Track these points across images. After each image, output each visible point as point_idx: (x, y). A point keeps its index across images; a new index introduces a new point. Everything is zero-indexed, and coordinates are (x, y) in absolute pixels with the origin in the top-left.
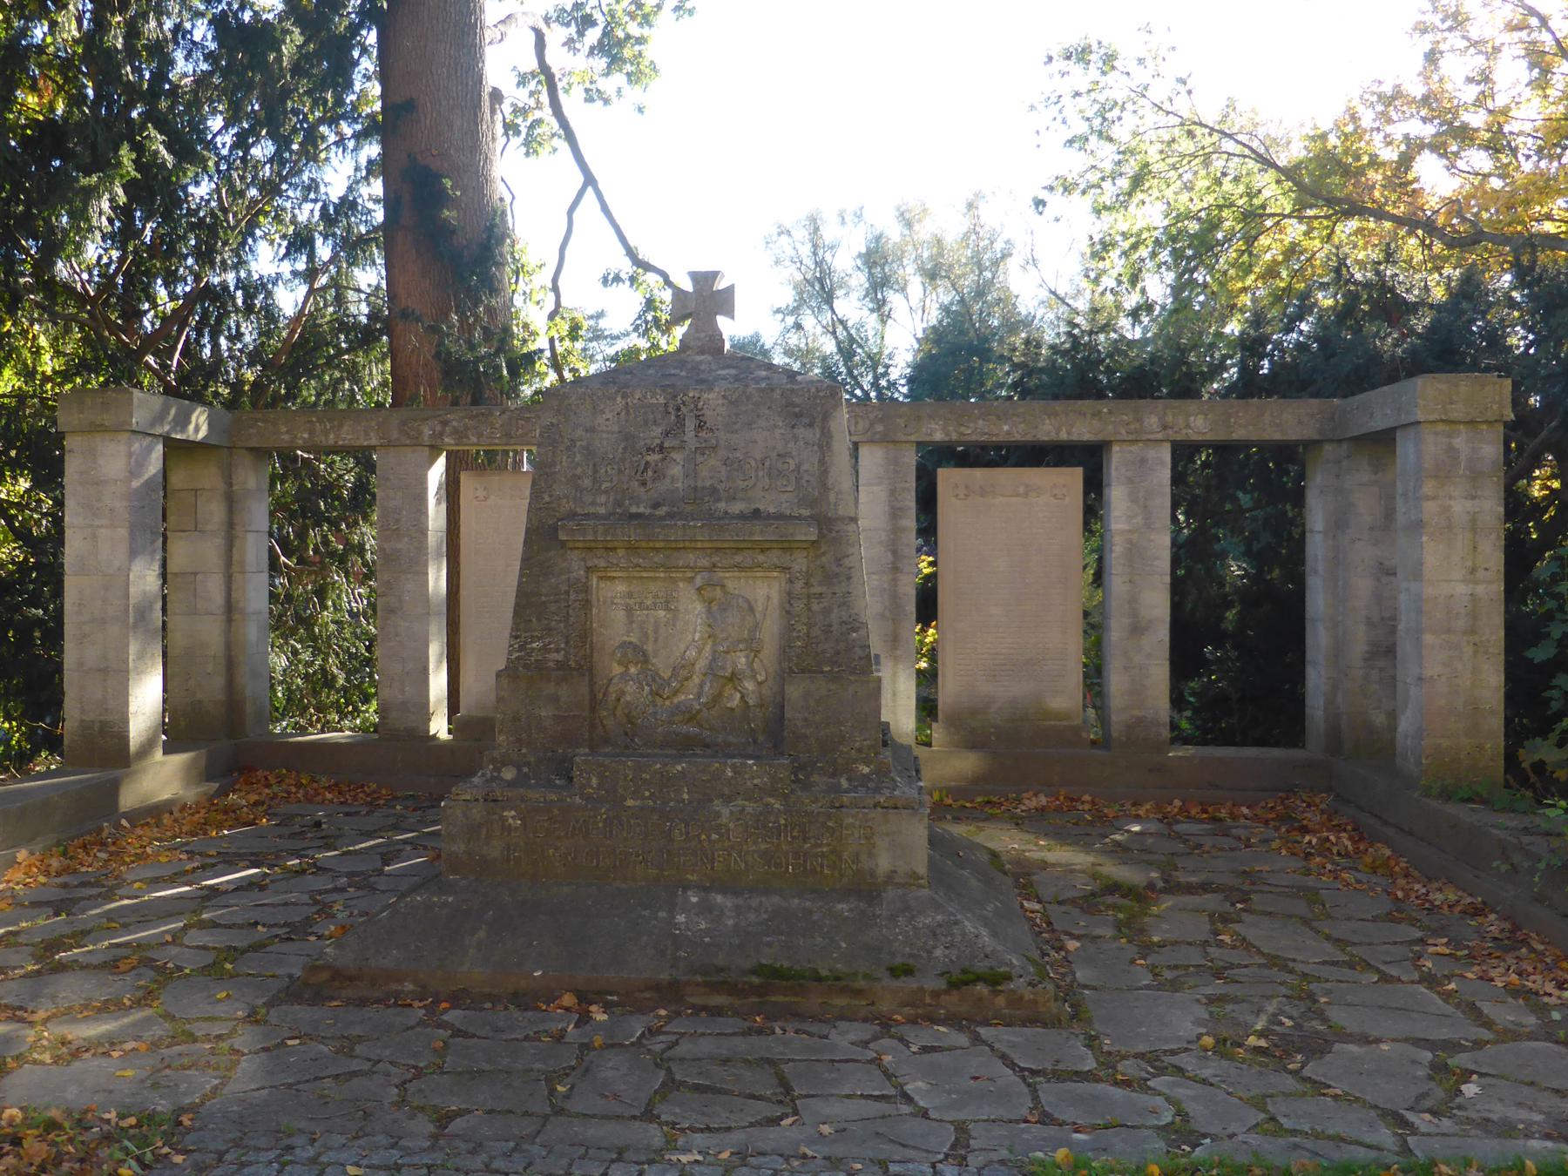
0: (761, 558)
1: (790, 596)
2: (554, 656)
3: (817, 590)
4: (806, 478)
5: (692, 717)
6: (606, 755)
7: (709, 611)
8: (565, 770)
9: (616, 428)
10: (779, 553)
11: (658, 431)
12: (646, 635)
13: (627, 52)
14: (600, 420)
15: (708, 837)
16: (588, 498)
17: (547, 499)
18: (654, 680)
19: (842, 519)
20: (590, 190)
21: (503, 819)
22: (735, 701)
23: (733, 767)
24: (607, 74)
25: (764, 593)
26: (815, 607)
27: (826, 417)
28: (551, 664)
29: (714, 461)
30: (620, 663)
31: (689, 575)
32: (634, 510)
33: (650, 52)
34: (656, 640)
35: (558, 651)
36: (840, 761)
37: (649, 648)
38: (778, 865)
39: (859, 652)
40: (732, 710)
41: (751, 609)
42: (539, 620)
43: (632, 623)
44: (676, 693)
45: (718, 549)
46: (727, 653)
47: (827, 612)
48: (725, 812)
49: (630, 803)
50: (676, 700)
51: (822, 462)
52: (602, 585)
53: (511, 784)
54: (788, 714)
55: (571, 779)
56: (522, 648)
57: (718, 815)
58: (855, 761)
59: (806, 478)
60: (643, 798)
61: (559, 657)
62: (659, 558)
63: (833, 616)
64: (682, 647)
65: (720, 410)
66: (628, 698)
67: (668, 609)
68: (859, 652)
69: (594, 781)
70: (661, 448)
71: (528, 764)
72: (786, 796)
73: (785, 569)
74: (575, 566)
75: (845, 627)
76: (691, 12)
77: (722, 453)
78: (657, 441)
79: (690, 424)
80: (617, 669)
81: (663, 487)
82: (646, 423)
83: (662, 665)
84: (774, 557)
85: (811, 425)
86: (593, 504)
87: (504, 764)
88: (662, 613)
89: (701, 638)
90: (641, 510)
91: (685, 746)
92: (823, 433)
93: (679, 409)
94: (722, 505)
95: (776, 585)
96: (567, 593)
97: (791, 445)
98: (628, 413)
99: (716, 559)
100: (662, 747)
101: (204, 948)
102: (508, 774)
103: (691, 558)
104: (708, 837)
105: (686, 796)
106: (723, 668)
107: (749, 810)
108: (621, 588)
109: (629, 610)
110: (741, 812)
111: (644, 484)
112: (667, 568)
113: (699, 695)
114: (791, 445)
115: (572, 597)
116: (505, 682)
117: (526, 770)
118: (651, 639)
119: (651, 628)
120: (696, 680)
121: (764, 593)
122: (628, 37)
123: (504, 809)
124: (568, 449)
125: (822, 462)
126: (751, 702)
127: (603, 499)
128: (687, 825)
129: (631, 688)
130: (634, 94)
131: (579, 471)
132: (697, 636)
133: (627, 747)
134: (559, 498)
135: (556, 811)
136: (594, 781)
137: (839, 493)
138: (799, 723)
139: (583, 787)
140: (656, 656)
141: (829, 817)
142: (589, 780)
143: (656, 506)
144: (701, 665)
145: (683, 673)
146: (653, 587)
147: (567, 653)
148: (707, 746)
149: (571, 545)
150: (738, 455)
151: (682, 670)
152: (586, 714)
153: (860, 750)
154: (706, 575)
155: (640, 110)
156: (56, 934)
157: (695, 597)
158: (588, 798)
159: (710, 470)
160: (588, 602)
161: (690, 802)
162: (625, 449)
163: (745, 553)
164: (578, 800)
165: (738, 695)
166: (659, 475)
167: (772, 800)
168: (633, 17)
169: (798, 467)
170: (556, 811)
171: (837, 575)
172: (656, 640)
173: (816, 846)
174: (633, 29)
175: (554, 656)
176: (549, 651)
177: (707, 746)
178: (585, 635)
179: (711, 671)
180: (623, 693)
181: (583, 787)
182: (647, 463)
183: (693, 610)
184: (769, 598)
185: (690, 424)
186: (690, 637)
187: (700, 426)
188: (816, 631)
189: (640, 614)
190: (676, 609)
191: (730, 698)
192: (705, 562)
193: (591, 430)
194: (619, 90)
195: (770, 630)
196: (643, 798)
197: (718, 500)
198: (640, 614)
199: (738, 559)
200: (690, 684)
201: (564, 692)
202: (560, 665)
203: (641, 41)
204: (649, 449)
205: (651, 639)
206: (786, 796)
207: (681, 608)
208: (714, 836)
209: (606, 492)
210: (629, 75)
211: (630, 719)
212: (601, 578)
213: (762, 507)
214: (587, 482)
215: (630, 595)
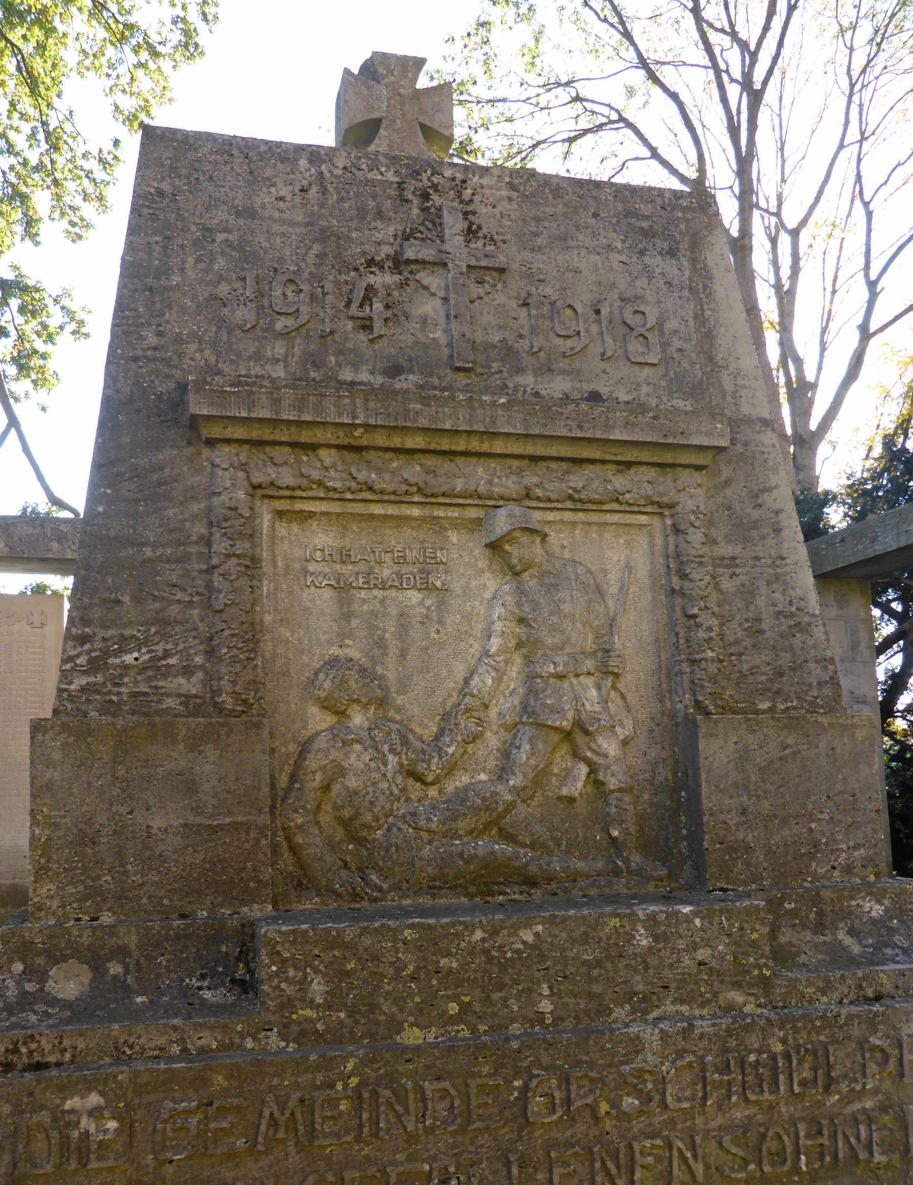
0: (620, 482)
1: (677, 565)
2: (180, 683)
3: (726, 550)
4: (676, 343)
5: (496, 822)
6: (308, 916)
7: (520, 592)
8: (235, 963)
9: (299, 216)
10: (650, 473)
11: (386, 231)
12: (381, 644)
13: (35, 362)
14: (263, 198)
15: (615, 1104)
16: (248, 346)
17: (152, 339)
18: (405, 742)
19: (749, 421)
20: (13, 431)
21: (64, 1121)
22: (577, 784)
23: (652, 921)
24: (17, 379)
25: (618, 559)
26: (727, 585)
27: (696, 243)
28: (170, 703)
29: (503, 298)
30: (327, 706)
31: (473, 513)
32: (347, 375)
33: (51, 365)
34: (403, 654)
35: (188, 671)
36: (826, 894)
37: (391, 672)
38: (779, 1156)
39: (816, 672)
40: (571, 800)
41: (599, 590)
42: (137, 600)
43: (348, 616)
44: (451, 769)
45: (535, 459)
46: (561, 677)
47: (748, 593)
48: (651, 1036)
49: (412, 1036)
50: (450, 787)
51: (700, 319)
52: (282, 530)
53: (78, 1012)
54: (709, 799)
55: (247, 987)
56: (94, 666)
57: (636, 1045)
58: (854, 891)
59: (676, 343)
60: (447, 1020)
61: (192, 685)
62: (414, 471)
63: (761, 601)
64: (460, 670)
65: (504, 206)
66: (352, 782)
67: (427, 588)
68: (816, 672)
69: (318, 988)
70: (398, 263)
71: (121, 953)
72: (766, 984)
73: (662, 507)
74: (224, 478)
75: (786, 623)
76: (87, 335)
77: (516, 284)
78: (387, 250)
79: (453, 224)
80: (319, 720)
81: (405, 335)
82: (362, 213)
83: (418, 709)
84: (639, 483)
85: (672, 253)
86: (257, 357)
87: (56, 957)
88: (414, 596)
89: (502, 650)
90: (364, 376)
91: (486, 882)
92: (694, 269)
93: (425, 196)
94: (528, 380)
95: (642, 541)
96: (207, 541)
97: (642, 283)
98: (324, 191)
99: (531, 479)
100: (433, 890)
101: (873, 133)
102: (69, 983)
103: (479, 475)
104: (615, 1104)
105: (546, 1006)
106: (558, 711)
107: (703, 1026)
108: (322, 538)
109: (343, 588)
110: (686, 1033)
111: (366, 325)
112: (429, 496)
113: (502, 773)
114: (642, 283)
115: (221, 546)
116: (54, 745)
117: (115, 968)
118: (393, 652)
119: (391, 628)
120: (493, 740)
121: (618, 559)
122: (35, 352)
123: (65, 1090)
124: (197, 244)
125: (700, 319)
126: (613, 783)
127: (279, 349)
128: (565, 1080)
129: (357, 758)
130: (40, 396)
131: (223, 289)
132: (495, 644)
133: (355, 896)
134: (178, 340)
135: (220, 1080)
136: (318, 988)
137: (736, 375)
138: (733, 819)
139: (288, 1004)
140: (403, 687)
141: (872, 1023)
142: (303, 984)
143: (394, 371)
144: (505, 705)
145: (468, 725)
146: (395, 539)
147: (210, 678)
148: (531, 882)
149: (216, 431)
150: (548, 291)
151: (461, 714)
152: (264, 819)
153: (848, 869)
154: (517, 510)
155: (43, 409)
156: (878, 451)
157: (482, 564)
158: (304, 1035)
159: (494, 315)
160: (255, 561)
161: (558, 1020)
162: (321, 256)
163: (590, 470)
164: (274, 1041)
165: (583, 770)
166: (396, 313)
167: (737, 997)
168: (39, 335)
169: (660, 323)
170: (220, 1080)
171: (756, 525)
172: (403, 654)
173: (847, 1100)
174: (39, 345)
175: (180, 683)
176: (167, 672)
177: (531, 882)
178: (251, 637)
179: (529, 714)
180: (341, 771)
181: (288, 1004)
182: (369, 288)
183: (480, 594)
184: (629, 567)
185: (453, 224)
186: (476, 648)
187: (471, 233)
188: (735, 631)
189: (366, 600)
190: (445, 590)
191: (567, 776)
192: (511, 485)
193: (249, 213)
194: (27, 394)
195: (637, 635)
196: (447, 1020)
197: (520, 370)
198: (366, 600)
199: (577, 479)
200: (480, 750)
201: (208, 766)
202: (192, 705)
203: (44, 356)
204: (371, 262)
205: (393, 652)
206: (766, 984)
207: (457, 588)
208: (630, 1102)
209: (285, 335)
210: (35, 382)
211: (353, 830)
212: (280, 514)
213: (604, 390)
214: (244, 314)
215: (345, 556)
